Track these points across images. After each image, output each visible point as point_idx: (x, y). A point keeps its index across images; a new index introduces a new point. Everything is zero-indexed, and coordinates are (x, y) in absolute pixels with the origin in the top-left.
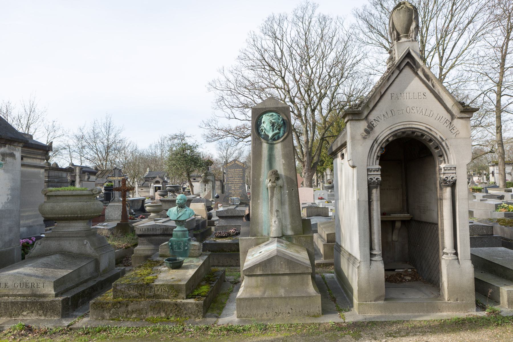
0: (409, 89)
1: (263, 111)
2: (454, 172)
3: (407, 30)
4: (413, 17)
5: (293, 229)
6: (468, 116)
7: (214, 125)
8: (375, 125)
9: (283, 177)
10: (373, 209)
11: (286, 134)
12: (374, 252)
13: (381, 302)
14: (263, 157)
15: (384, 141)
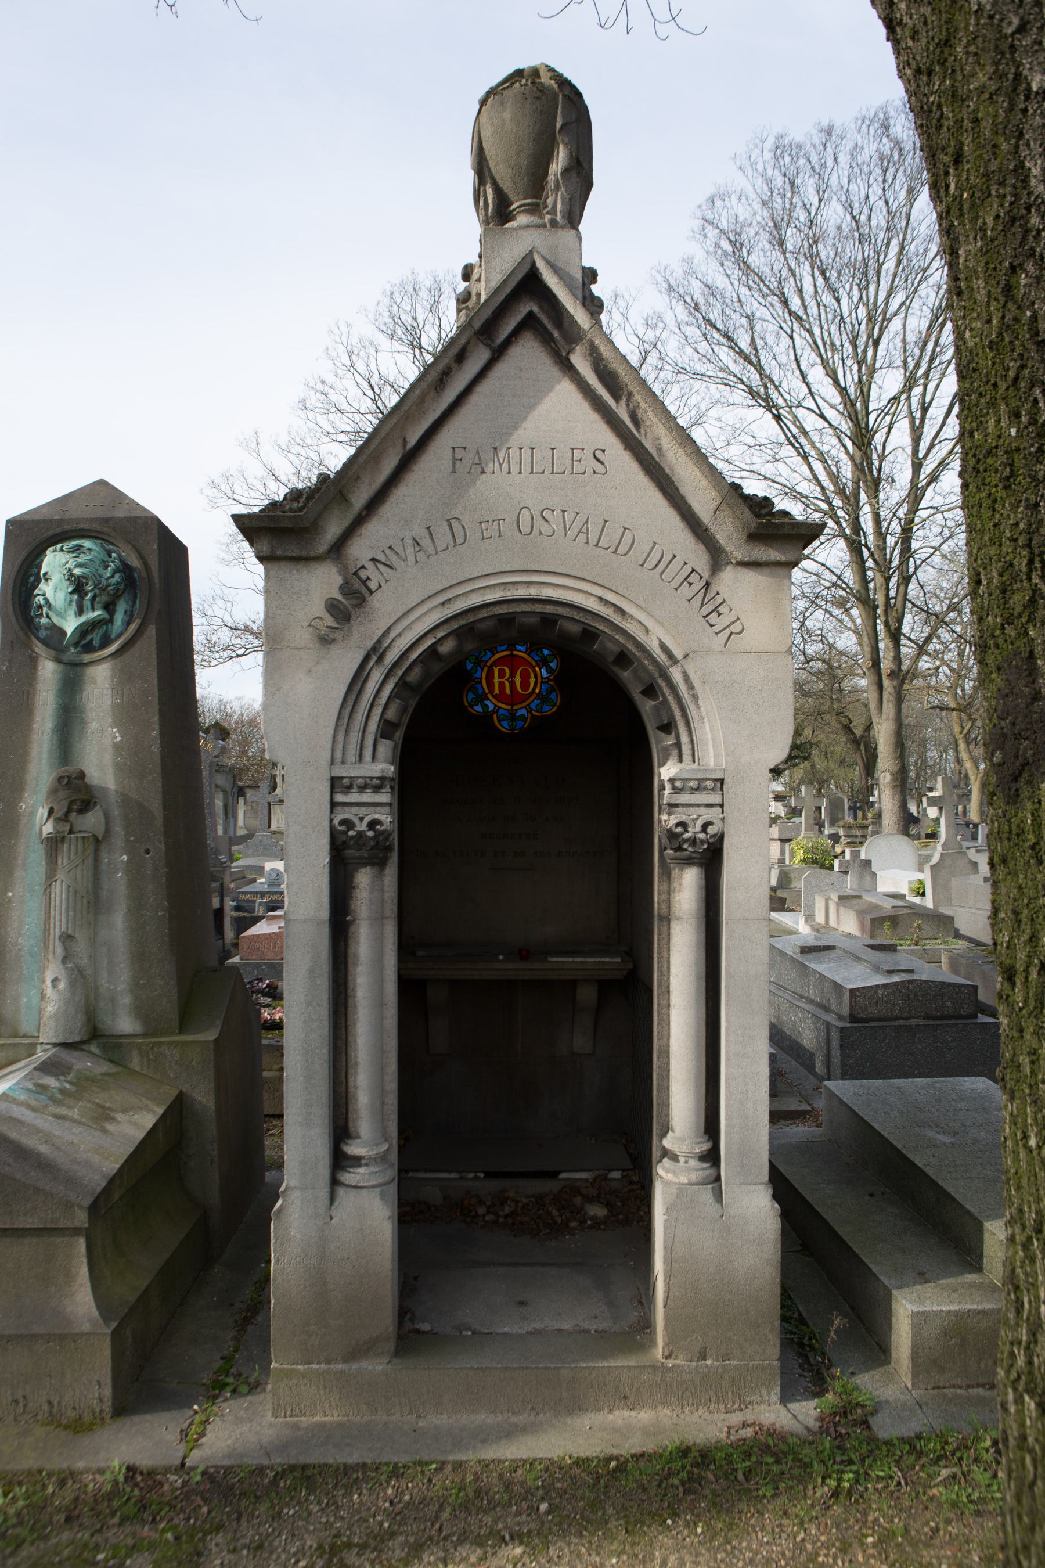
0: (528, 432)
1: (50, 533)
2: (716, 799)
3: (536, 183)
4: (558, 125)
5: (142, 1011)
6: (782, 558)
7: (219, 613)
8: (373, 585)
9: (113, 798)
10: (356, 956)
11: (133, 627)
12: (354, 1149)
13: (376, 1366)
14: (38, 717)
15: (414, 655)
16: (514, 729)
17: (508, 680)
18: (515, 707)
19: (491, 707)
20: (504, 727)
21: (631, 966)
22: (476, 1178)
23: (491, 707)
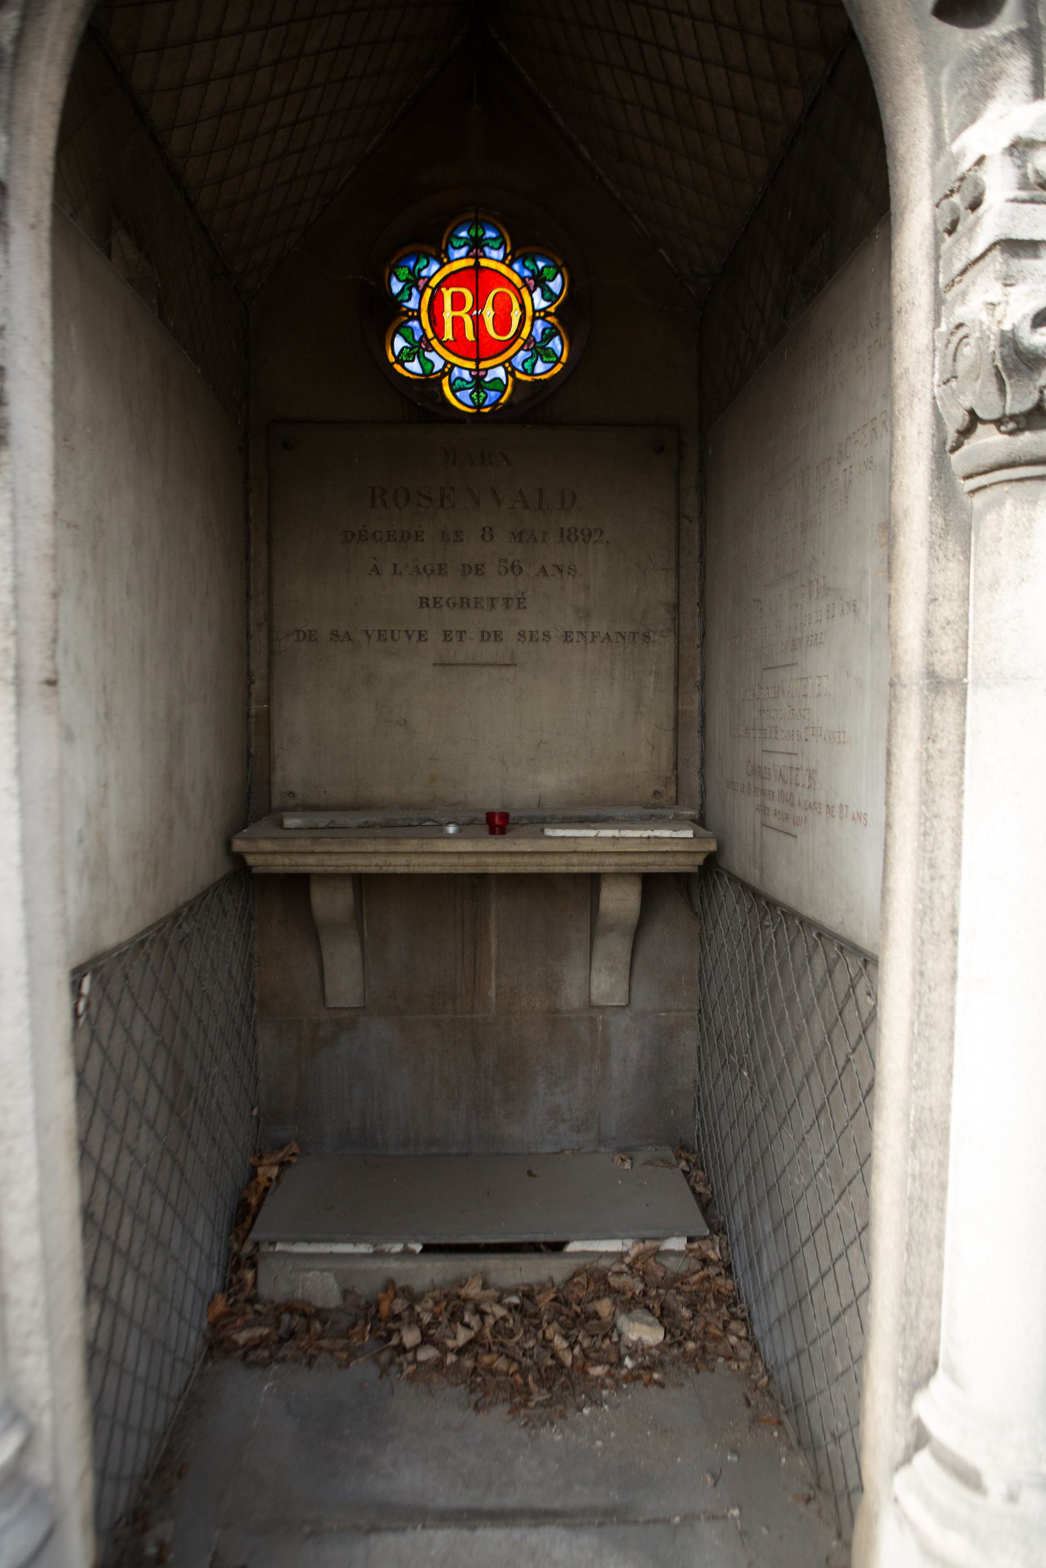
16: (479, 406)
17: (470, 313)
18: (483, 365)
19: (439, 364)
20: (461, 401)
21: (712, 847)
22: (407, 1253)
23: (439, 364)
